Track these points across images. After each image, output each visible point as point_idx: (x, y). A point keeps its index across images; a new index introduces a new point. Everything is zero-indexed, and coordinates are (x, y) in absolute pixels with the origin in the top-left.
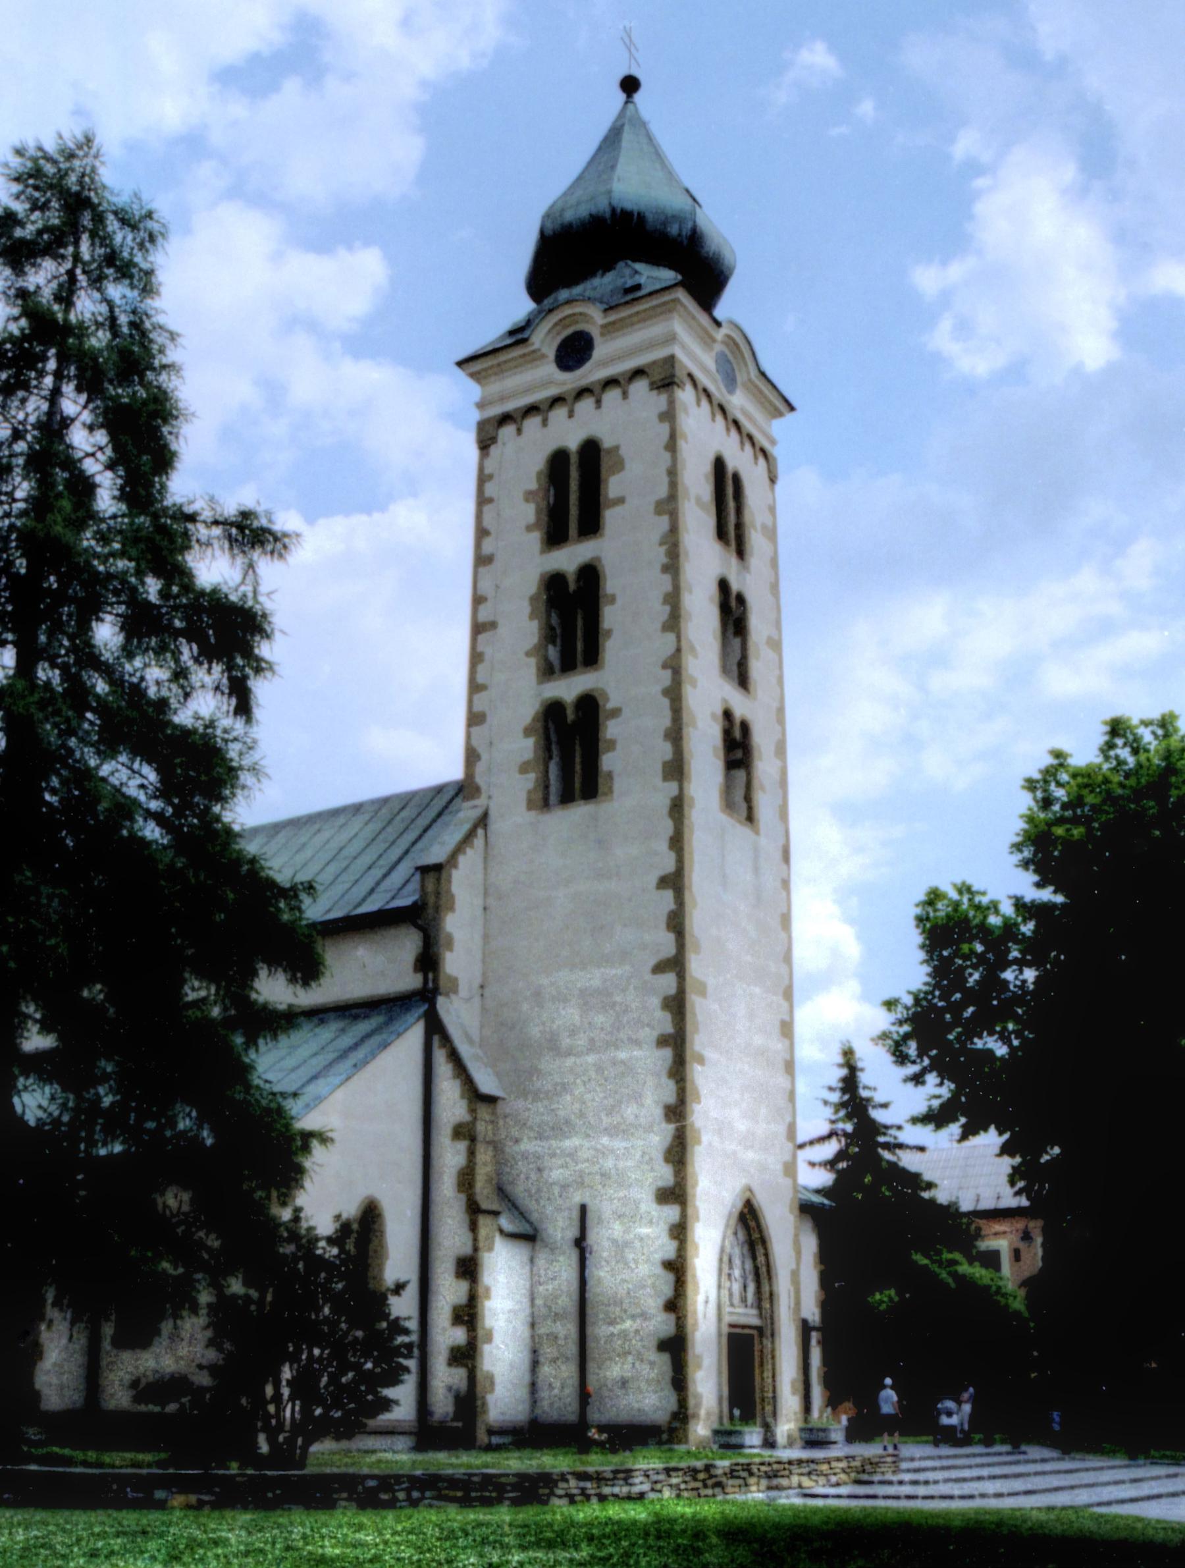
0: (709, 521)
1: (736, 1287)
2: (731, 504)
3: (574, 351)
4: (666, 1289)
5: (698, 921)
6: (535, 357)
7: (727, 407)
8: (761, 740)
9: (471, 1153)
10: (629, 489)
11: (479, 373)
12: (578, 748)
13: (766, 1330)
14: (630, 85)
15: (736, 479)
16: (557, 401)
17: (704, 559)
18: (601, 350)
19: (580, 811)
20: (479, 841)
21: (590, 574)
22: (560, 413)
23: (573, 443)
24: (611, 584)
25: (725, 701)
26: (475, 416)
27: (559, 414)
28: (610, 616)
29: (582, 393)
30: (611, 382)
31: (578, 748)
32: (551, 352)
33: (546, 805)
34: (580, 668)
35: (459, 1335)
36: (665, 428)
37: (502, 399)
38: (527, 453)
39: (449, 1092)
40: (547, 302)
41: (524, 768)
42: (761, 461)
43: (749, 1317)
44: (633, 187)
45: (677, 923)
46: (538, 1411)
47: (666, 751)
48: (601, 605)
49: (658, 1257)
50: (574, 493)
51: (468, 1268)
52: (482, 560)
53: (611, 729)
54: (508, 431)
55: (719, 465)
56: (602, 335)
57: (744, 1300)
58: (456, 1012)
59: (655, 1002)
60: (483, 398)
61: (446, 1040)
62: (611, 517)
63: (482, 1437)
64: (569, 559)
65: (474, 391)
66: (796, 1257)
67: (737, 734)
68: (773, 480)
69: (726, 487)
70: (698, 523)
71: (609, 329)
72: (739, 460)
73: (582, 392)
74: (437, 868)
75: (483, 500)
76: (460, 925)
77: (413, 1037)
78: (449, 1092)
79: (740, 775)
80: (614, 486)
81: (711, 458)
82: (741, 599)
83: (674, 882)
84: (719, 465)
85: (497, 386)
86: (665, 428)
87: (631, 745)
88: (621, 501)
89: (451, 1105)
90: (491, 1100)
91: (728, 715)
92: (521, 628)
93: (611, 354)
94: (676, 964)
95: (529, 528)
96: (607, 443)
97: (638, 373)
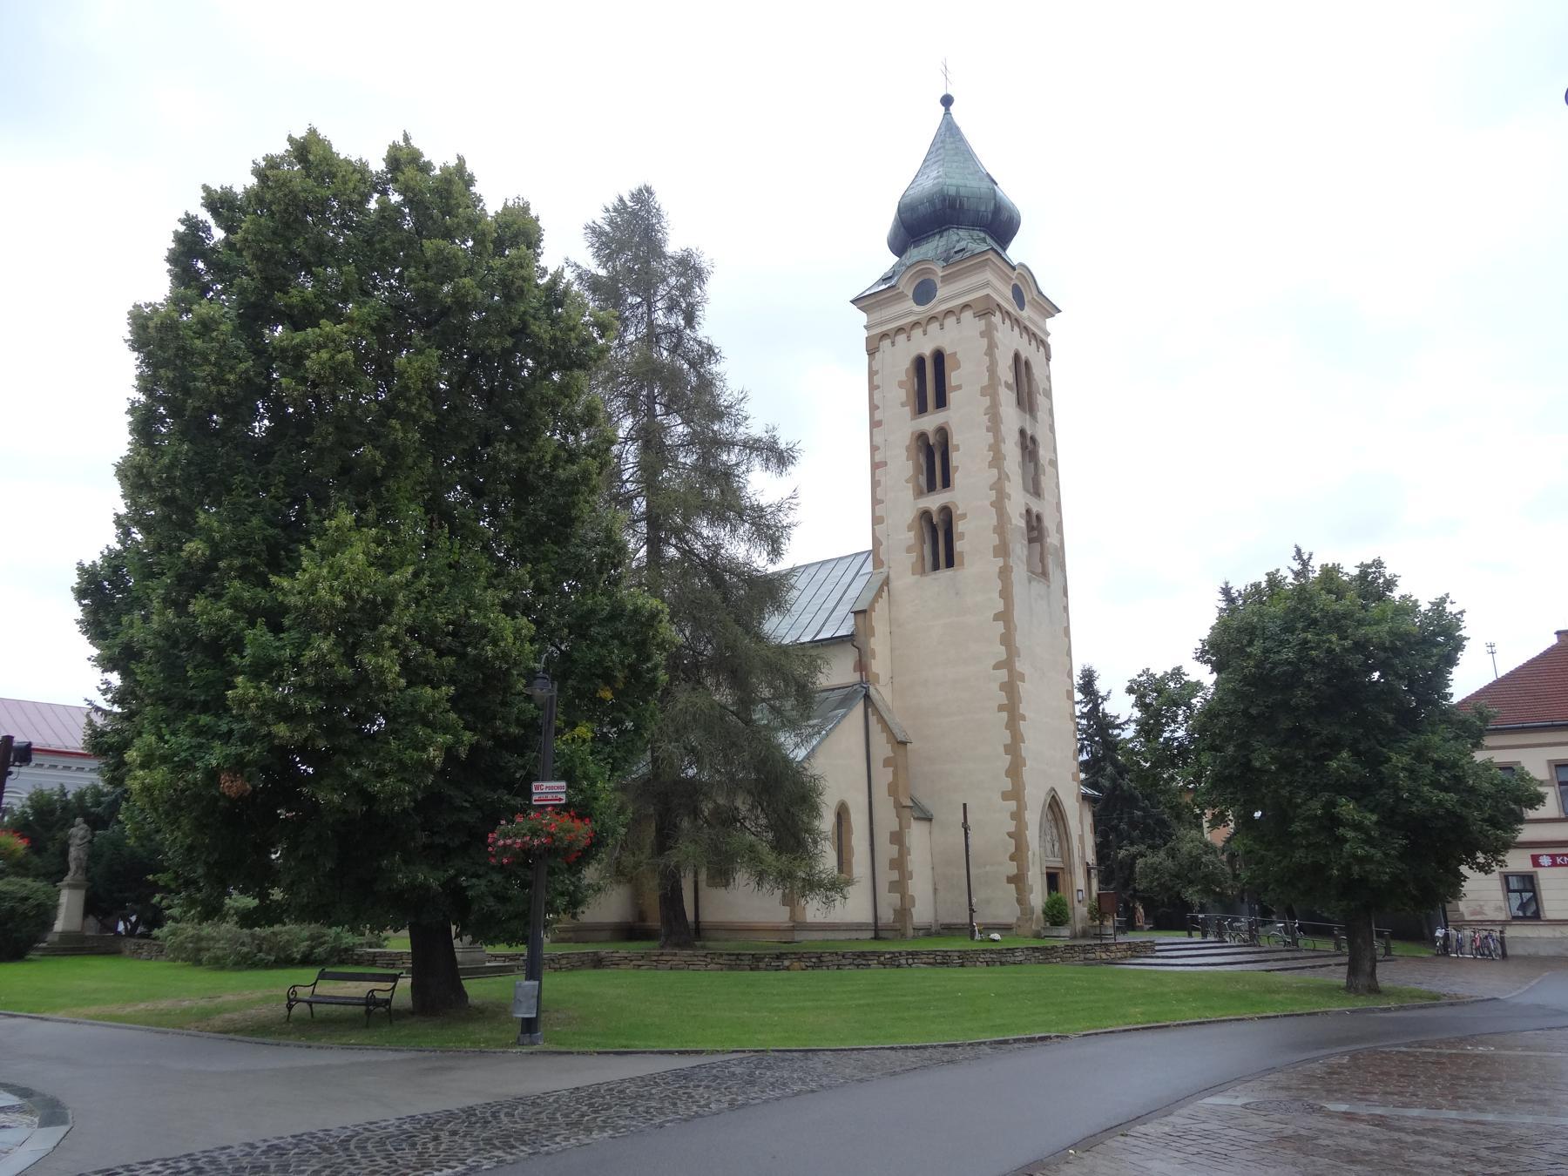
1: (1049, 846)
2: (1025, 379)
3: (924, 293)
4: (1011, 845)
5: (1020, 640)
6: (901, 297)
8: (1048, 523)
9: (895, 774)
10: (965, 379)
13: (1068, 869)
14: (947, 101)
15: (1027, 363)
16: (916, 324)
18: (942, 292)
19: (944, 574)
20: (885, 594)
21: (943, 433)
22: (917, 332)
23: (927, 351)
24: (956, 439)
26: (865, 334)
28: (955, 459)
29: (933, 318)
30: (949, 312)
33: (923, 572)
35: (895, 876)
36: (985, 342)
37: (881, 323)
39: (879, 738)
41: (909, 550)
43: (1056, 862)
44: (956, 181)
45: (1007, 640)
47: (995, 539)
50: (931, 381)
51: (898, 838)
52: (875, 424)
53: (960, 527)
54: (887, 342)
55: (1017, 357)
57: (1053, 853)
58: (883, 693)
59: (995, 686)
61: (877, 711)
62: (953, 397)
63: (910, 932)
65: (862, 318)
66: (1080, 824)
68: (1048, 358)
69: (1021, 367)
70: (1007, 398)
71: (945, 279)
72: (1029, 351)
74: (864, 612)
75: (873, 387)
76: (879, 644)
77: (858, 710)
78: (879, 738)
79: (1037, 546)
80: (953, 378)
81: (1012, 354)
82: (1033, 439)
83: (1005, 616)
85: (880, 315)
86: (985, 342)
87: (973, 535)
88: (959, 387)
89: (881, 748)
90: (904, 743)
91: (1028, 512)
92: (903, 466)
93: (947, 294)
94: (1007, 664)
95: (903, 405)
96: (948, 351)
97: (966, 306)
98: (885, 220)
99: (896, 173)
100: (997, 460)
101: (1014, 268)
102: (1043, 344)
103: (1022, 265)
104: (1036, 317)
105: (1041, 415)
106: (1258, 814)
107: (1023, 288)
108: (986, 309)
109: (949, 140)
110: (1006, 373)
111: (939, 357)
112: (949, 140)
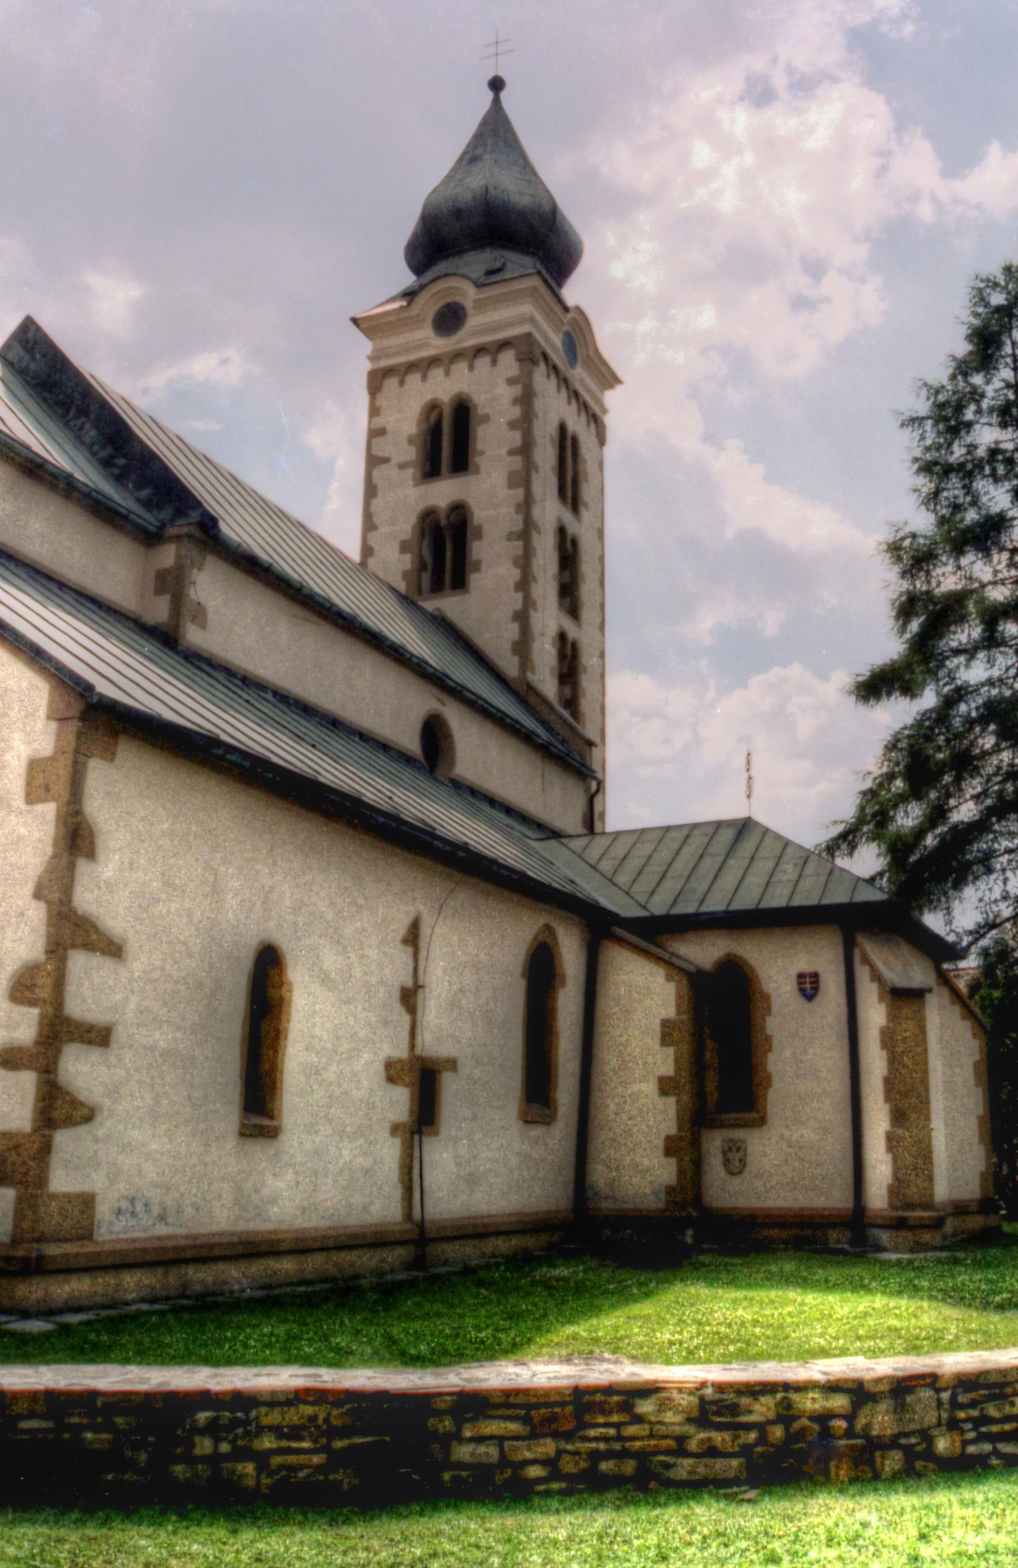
0: (553, 481)
3: (450, 318)
7: (570, 379)
8: (588, 660)
10: (493, 441)
11: (80, 1238)
12: (370, 1439)
14: (497, 85)
15: (575, 440)
17: (549, 510)
18: (474, 321)
25: (561, 626)
26: (367, 366)
27: (437, 374)
31: (370, 1439)
32: (431, 314)
34: (448, 591)
38: (407, 410)
40: (429, 275)
42: (593, 426)
46: (418, 1051)
48: (467, 571)
49: (511, 583)
55: (562, 429)
56: (474, 308)
60: (374, 351)
64: (443, 493)
65: (366, 346)
67: (569, 651)
69: (567, 446)
70: (545, 482)
71: (481, 305)
72: (577, 425)
73: (457, 355)
82: (574, 542)
84: (562, 429)
98: (406, 224)
99: (425, 166)
100: (525, 563)
101: (566, 309)
102: (595, 420)
103: (578, 309)
104: (593, 386)
105: (587, 614)
106: (1006, 1146)
107: (578, 336)
108: (529, 353)
109: (495, 133)
110: (546, 456)
111: (463, 413)
112: (495, 133)
